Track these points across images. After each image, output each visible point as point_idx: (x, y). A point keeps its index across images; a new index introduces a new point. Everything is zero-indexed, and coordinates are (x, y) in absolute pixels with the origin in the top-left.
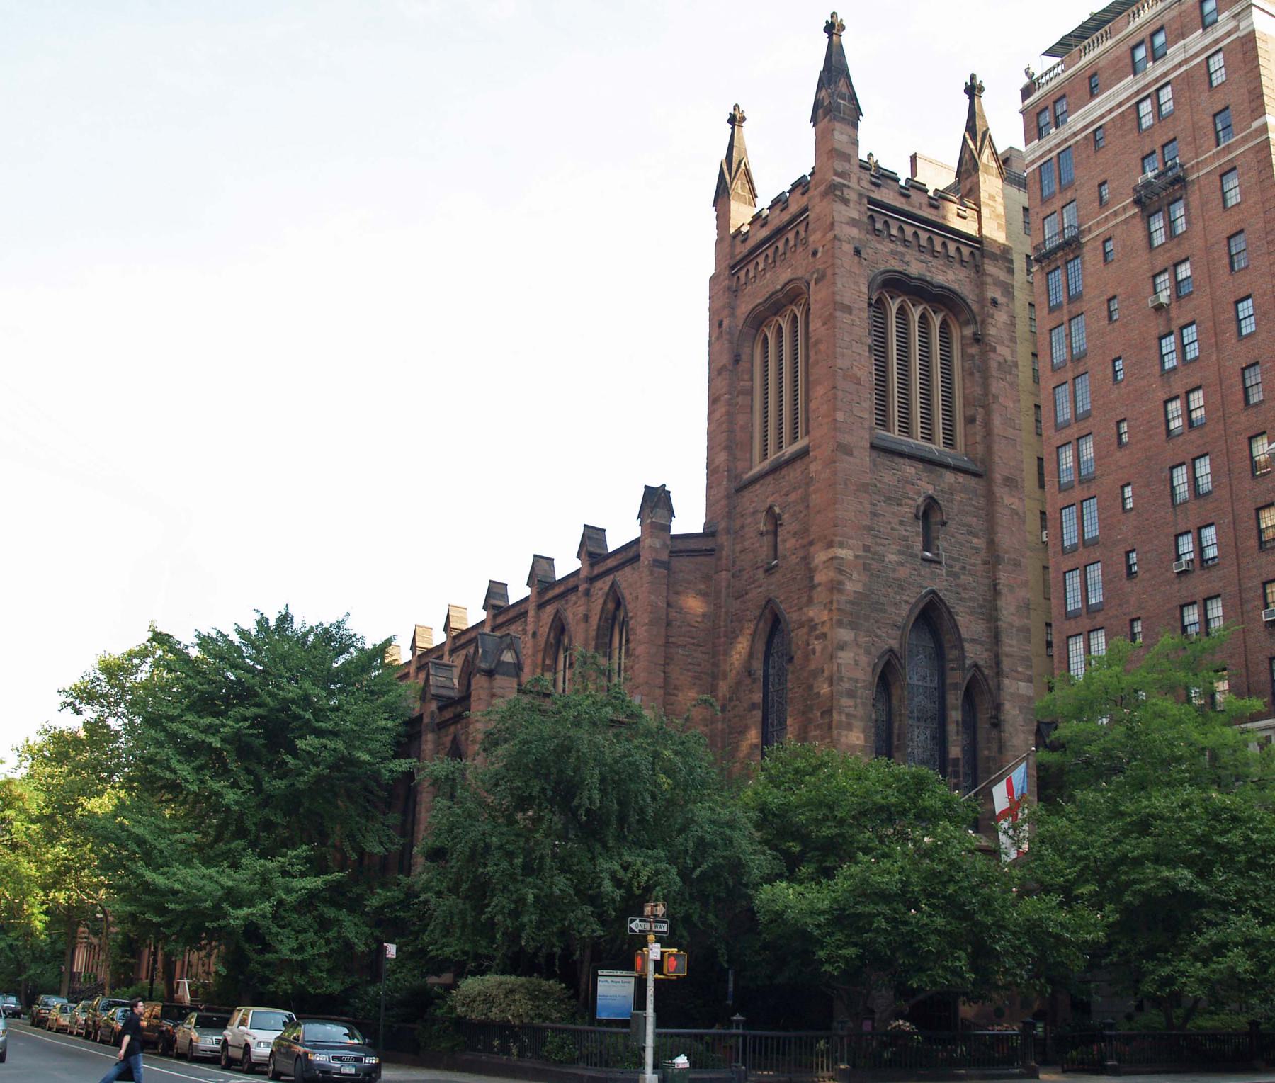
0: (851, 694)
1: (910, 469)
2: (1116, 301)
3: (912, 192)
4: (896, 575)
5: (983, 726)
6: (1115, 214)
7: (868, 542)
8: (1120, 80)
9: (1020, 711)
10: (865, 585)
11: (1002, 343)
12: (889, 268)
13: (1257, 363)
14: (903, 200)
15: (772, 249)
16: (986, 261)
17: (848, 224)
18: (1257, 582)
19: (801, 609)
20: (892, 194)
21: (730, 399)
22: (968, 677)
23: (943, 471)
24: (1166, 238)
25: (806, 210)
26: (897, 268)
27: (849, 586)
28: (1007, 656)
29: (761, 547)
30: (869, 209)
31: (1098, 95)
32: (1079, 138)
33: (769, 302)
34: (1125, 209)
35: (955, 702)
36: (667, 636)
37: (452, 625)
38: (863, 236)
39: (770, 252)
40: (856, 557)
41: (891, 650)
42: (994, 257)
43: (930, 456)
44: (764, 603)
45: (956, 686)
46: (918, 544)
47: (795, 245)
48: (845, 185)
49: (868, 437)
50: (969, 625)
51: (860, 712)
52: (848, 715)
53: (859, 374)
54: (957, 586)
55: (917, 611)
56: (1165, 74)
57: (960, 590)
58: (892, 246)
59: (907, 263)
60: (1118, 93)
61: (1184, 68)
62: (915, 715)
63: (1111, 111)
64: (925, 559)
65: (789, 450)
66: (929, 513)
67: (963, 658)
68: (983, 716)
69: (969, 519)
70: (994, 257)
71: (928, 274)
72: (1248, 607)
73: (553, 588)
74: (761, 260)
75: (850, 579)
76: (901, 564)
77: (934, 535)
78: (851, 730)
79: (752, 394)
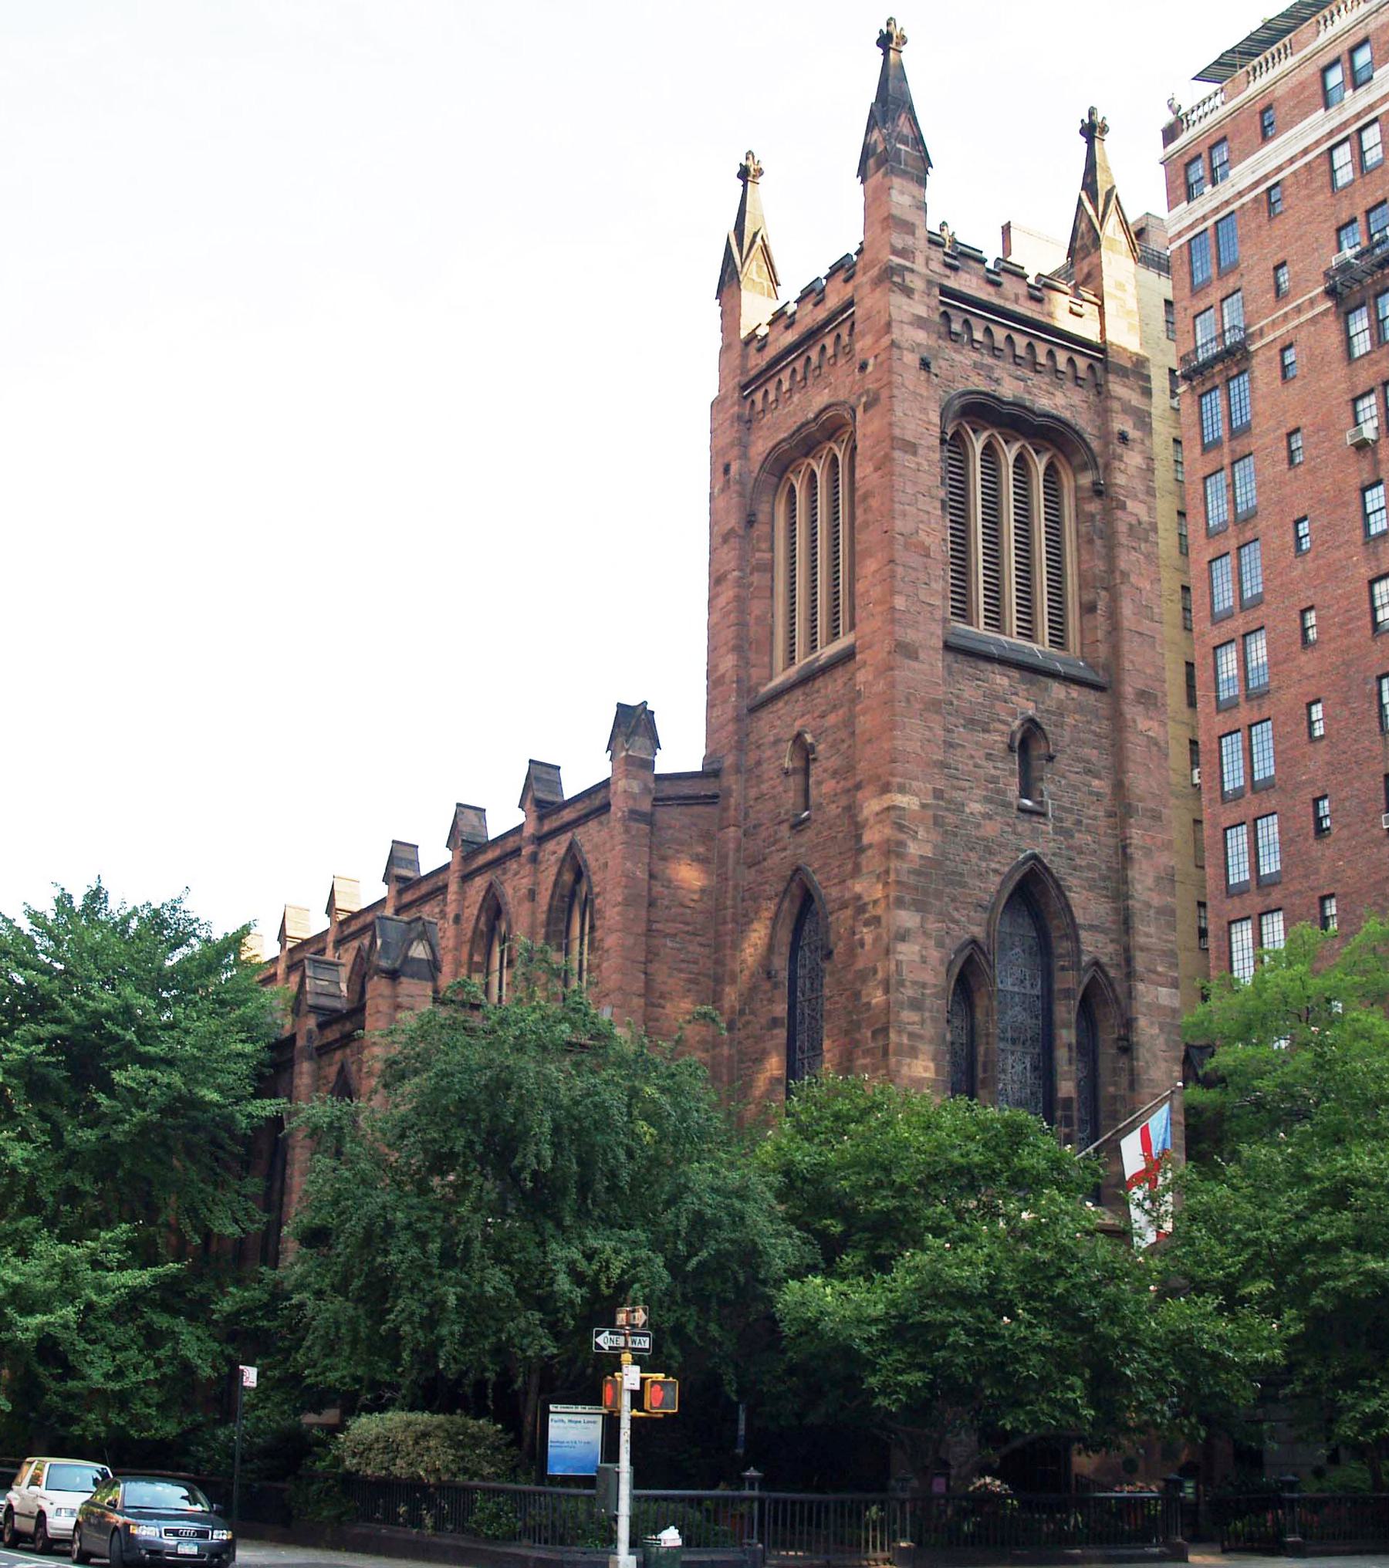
0: (916, 1005)
1: (1001, 680)
2: (1299, 435)
3: (1004, 279)
4: (982, 833)
5: (1107, 1051)
6: (1299, 310)
8: (1306, 115)
9: (1161, 1030)
10: (935, 846)
11: (1135, 497)
14: (991, 289)
15: (802, 360)
16: (1111, 377)
17: (911, 324)
20: (974, 280)
23: (1050, 682)
24: (1372, 345)
25: (850, 304)
26: (982, 388)
27: (913, 849)
28: (1142, 949)
31: (1273, 138)
33: (797, 438)
34: (1312, 302)
36: (650, 921)
39: (799, 365)
40: (924, 806)
41: (974, 941)
42: (1123, 372)
43: (1030, 660)
45: (1068, 993)
49: (940, 632)
51: (929, 1031)
52: (911, 1035)
53: (928, 541)
54: (1069, 848)
55: (1011, 886)
56: (1371, 108)
57: (1073, 854)
58: (975, 356)
64: (1023, 810)
65: (826, 652)
67: (1079, 952)
68: (1108, 1036)
70: (1123, 372)
71: (1026, 396)
73: (485, 852)
75: (915, 838)
76: (988, 816)
78: (916, 1058)
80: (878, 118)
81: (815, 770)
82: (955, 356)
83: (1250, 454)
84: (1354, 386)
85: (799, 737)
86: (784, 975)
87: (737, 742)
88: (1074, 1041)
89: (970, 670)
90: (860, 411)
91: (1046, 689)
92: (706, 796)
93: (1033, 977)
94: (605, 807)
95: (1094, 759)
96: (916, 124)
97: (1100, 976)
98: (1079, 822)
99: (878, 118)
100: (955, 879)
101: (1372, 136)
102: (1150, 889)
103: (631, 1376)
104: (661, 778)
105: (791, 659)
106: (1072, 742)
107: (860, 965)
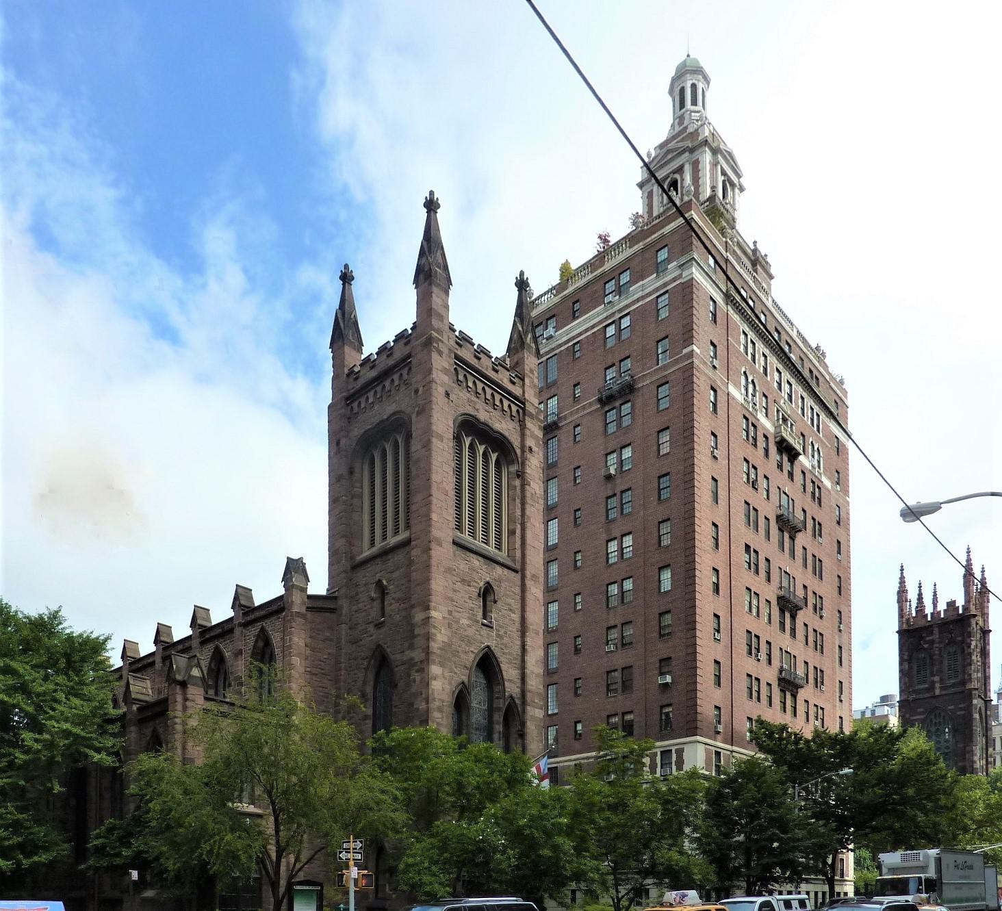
0: (440, 709)
1: (476, 562)
2: (579, 470)
3: (482, 356)
4: (466, 633)
5: (514, 736)
6: (584, 408)
10: (448, 637)
11: (534, 480)
13: (668, 519)
14: (476, 360)
16: (527, 418)
19: (403, 652)
24: (617, 429)
25: (409, 356)
26: (472, 413)
28: (529, 692)
29: (372, 608)
30: (456, 363)
31: (578, 317)
32: (562, 348)
35: (499, 719)
37: (128, 654)
39: (379, 389)
40: (444, 618)
43: (487, 553)
44: (374, 647)
47: (381, 397)
49: (451, 534)
50: (509, 672)
51: (444, 722)
52: (438, 723)
54: (502, 644)
56: (627, 306)
57: (503, 647)
59: (477, 410)
60: (590, 319)
63: (586, 330)
64: (483, 624)
65: (393, 540)
66: (487, 593)
67: (504, 691)
68: (514, 730)
69: (510, 601)
73: (253, 613)
74: (371, 394)
75: (440, 633)
79: (362, 497)
80: (426, 250)
81: (388, 599)
83: (556, 477)
84: (606, 448)
85: (379, 582)
88: (501, 730)
89: (463, 555)
90: (414, 416)
94: (153, 663)
95: (513, 605)
96: (446, 259)
98: (506, 633)
99: (426, 250)
100: (455, 653)
101: (626, 322)
103: (354, 872)
104: (311, 597)
105: (372, 543)
107: (414, 689)
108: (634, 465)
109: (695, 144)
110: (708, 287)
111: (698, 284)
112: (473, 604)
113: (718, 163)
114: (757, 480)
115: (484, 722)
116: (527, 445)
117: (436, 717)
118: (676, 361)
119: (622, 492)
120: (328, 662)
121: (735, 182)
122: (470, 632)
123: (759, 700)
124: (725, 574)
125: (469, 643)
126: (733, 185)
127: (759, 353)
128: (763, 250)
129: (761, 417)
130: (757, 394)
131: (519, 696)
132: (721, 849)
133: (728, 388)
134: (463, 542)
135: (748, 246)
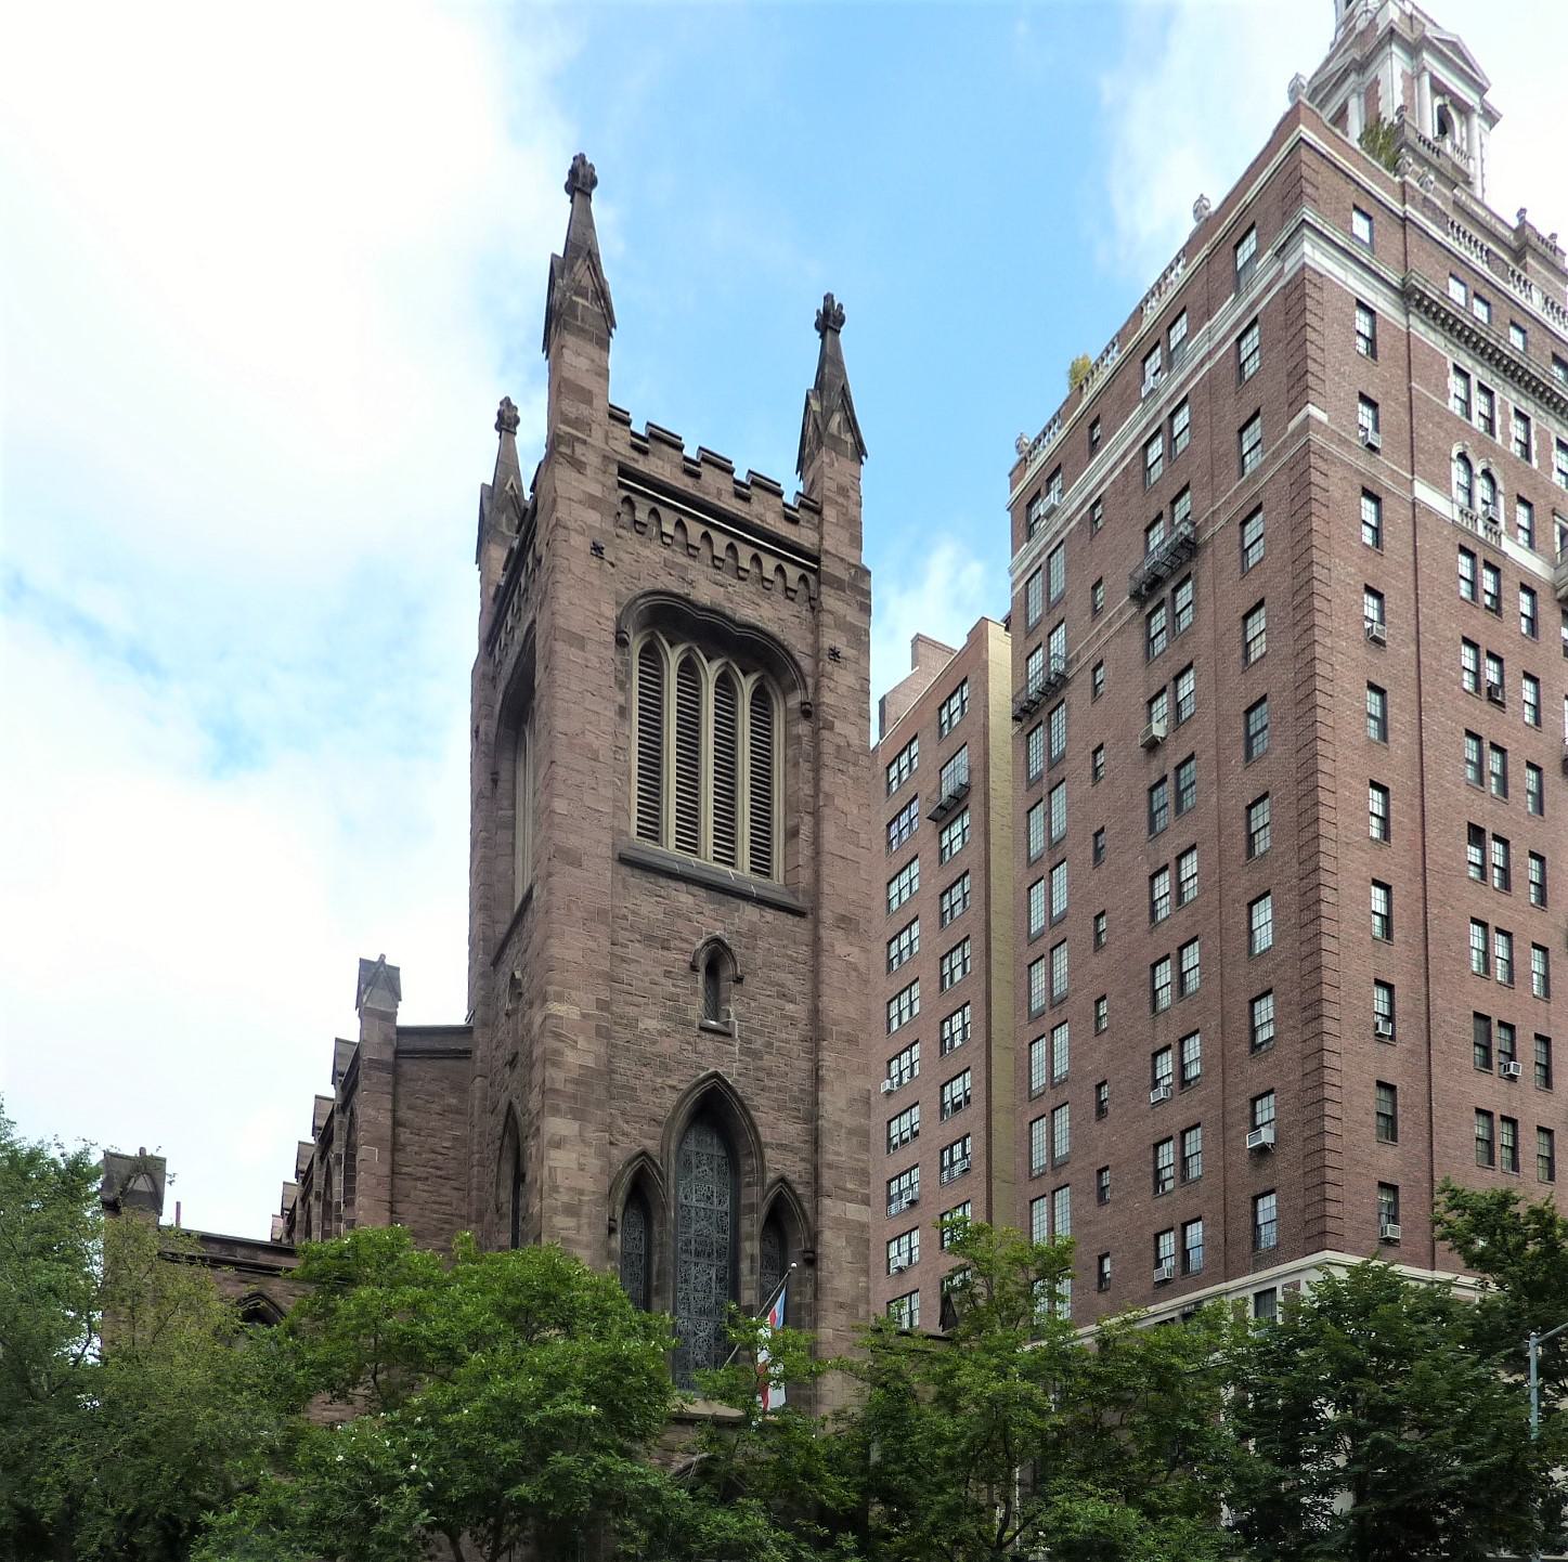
0: (571, 1210)
1: (684, 897)
3: (705, 470)
4: (656, 1049)
6: (1109, 624)
7: (605, 995)
9: (847, 1242)
10: (597, 1057)
11: (845, 718)
12: (659, 586)
14: (688, 480)
16: (824, 588)
18: (1244, 1101)
20: (668, 467)
21: (488, 838)
22: (771, 1195)
23: (742, 904)
27: (571, 1057)
30: (621, 485)
32: (1073, 523)
34: (1121, 613)
38: (608, 525)
40: (584, 1016)
42: (838, 584)
43: (725, 881)
45: (752, 1208)
46: (696, 1009)
48: (578, 439)
50: (775, 1127)
53: (596, 744)
54: (757, 1069)
55: (689, 1102)
57: (761, 1075)
58: (666, 553)
59: (691, 583)
60: (1118, 443)
61: (1207, 367)
62: (693, 1247)
63: (1112, 470)
66: (716, 962)
67: (763, 1169)
70: (838, 584)
71: (727, 604)
72: (1233, 1133)
75: (574, 1048)
77: (723, 996)
79: (514, 828)
82: (640, 549)
83: (1064, 780)
86: (507, 1208)
87: (483, 997)
89: (648, 885)
91: (737, 910)
92: (460, 1052)
93: (721, 1195)
97: (786, 1193)
98: (769, 1045)
102: (843, 1111)
106: (764, 965)
108: (1199, 704)
109: (1368, 50)
110: (1352, 281)
111: (1321, 276)
112: (673, 985)
113: (1424, 69)
114: (1502, 685)
115: (718, 1238)
116: (826, 646)
117: (560, 1225)
118: (1276, 455)
119: (1179, 768)
120: (452, 1153)
121: (1471, 103)
122: (666, 1045)
123: (1515, 1166)
124: (1409, 893)
125: (666, 1069)
126: (1465, 110)
127: (1505, 413)
128: (1543, 225)
129: (1515, 550)
130: (1501, 499)
131: (806, 1178)
132: (1250, 1491)
133: (1412, 492)
134: (706, 875)
135: (1502, 222)
